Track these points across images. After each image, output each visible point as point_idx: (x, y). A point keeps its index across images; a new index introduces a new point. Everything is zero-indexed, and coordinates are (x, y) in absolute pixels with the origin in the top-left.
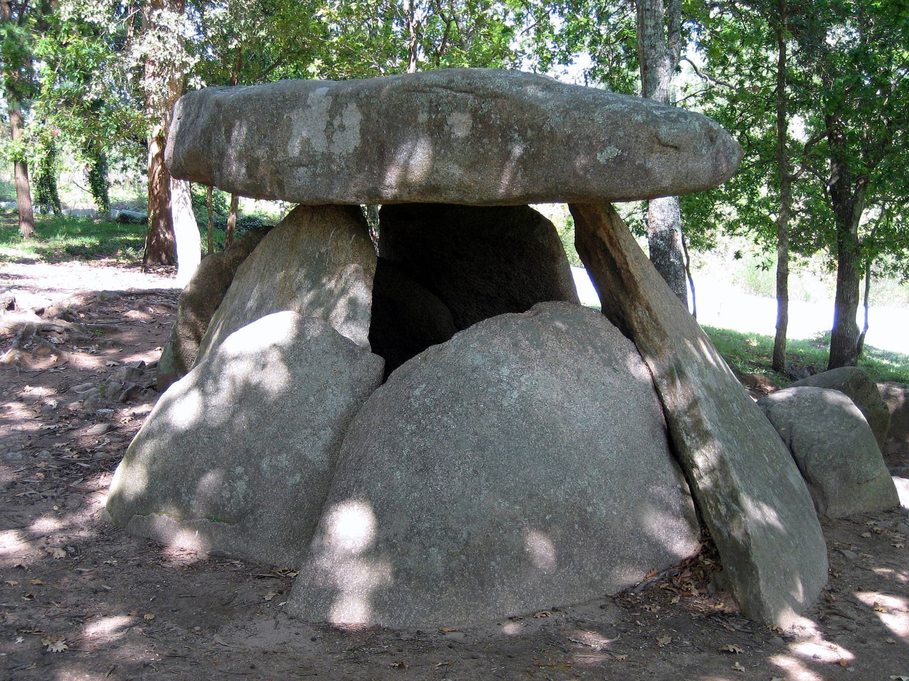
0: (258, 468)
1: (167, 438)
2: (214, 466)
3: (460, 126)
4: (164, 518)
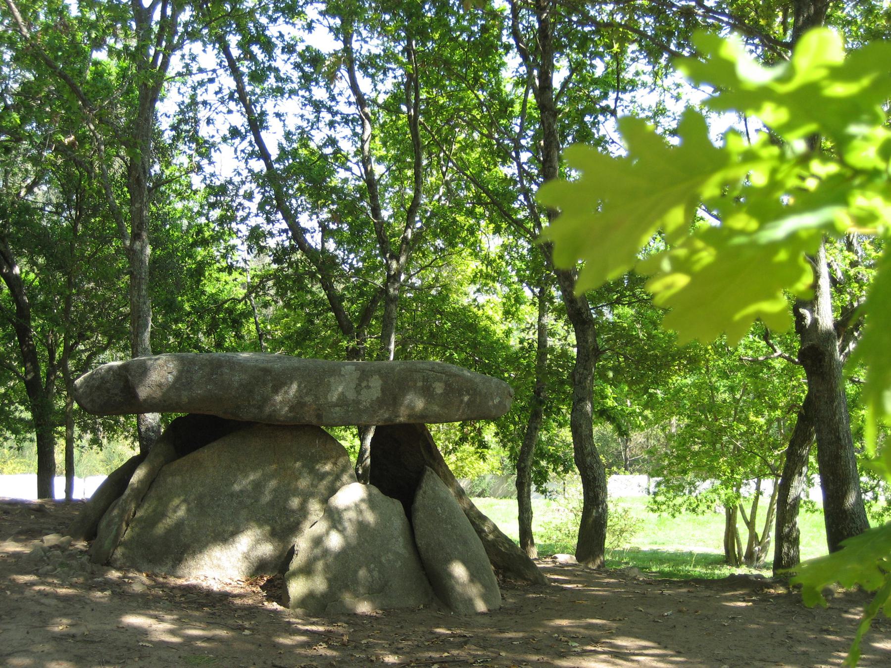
0: (381, 562)
1: (330, 559)
2: (360, 567)
3: (439, 388)
4: (348, 598)
